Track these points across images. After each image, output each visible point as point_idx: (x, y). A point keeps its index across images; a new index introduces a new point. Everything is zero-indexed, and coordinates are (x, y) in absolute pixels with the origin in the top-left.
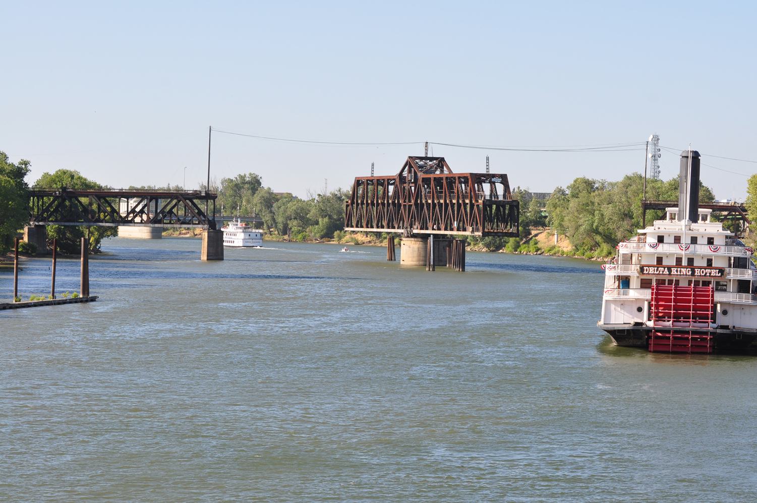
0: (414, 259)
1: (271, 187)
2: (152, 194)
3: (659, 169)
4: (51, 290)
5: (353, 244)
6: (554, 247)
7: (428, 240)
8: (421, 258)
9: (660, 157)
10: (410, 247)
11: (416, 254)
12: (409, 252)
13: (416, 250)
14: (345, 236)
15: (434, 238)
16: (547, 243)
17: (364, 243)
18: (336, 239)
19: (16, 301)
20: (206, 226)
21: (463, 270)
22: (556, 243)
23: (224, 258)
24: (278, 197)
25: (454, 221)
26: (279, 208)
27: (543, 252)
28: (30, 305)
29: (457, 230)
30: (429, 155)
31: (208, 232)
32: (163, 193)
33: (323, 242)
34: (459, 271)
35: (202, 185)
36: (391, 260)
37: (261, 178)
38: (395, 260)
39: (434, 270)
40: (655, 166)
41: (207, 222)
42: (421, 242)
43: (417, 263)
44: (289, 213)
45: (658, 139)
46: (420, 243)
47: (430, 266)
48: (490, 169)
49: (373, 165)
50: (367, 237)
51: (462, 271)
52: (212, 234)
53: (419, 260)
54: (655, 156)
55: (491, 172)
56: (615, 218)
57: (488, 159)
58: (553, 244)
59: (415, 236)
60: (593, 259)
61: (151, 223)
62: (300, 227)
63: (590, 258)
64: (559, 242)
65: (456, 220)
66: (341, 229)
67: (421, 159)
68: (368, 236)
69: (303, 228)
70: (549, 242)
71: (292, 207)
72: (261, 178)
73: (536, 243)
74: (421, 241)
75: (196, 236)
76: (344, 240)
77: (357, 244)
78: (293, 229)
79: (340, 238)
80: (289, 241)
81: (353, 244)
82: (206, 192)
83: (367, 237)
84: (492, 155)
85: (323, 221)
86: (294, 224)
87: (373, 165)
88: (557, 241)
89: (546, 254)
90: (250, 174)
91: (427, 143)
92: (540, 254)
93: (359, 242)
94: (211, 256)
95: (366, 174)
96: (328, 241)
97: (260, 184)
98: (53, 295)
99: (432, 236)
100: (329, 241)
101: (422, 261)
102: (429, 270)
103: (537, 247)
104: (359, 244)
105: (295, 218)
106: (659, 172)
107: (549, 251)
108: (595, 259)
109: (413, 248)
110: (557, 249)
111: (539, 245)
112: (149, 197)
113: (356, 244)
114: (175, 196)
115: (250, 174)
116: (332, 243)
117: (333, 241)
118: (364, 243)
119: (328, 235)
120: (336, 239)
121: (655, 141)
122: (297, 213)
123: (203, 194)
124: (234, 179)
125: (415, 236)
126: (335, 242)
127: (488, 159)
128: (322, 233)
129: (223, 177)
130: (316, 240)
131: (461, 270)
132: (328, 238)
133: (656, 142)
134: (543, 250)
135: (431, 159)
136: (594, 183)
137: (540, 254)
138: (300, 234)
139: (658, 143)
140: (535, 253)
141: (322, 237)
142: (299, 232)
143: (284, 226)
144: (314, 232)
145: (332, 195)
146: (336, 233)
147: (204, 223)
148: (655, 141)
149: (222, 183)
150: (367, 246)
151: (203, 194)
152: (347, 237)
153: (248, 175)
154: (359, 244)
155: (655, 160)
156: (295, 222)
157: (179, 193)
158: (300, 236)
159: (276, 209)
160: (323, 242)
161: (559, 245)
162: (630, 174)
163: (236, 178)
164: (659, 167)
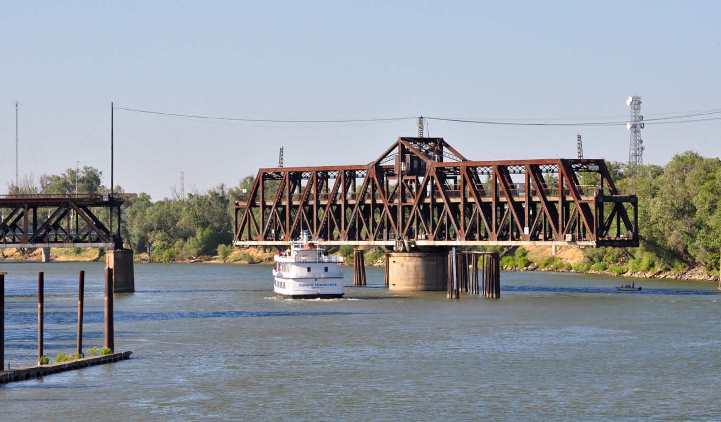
0: (410, 283)
1: (121, 186)
2: (32, 202)
3: (643, 145)
4: (38, 344)
5: (246, 262)
6: (552, 260)
7: (449, 256)
8: (420, 281)
9: (643, 128)
10: (402, 265)
11: (412, 275)
12: (402, 272)
13: (412, 269)
14: (232, 252)
15: (457, 251)
16: (540, 254)
17: (261, 261)
18: (220, 255)
19: (42, 363)
20: (111, 244)
21: (498, 296)
22: (554, 253)
23: (136, 289)
24: (130, 199)
25: (523, 226)
26: (134, 214)
27: (537, 267)
28: (64, 367)
29: (531, 240)
30: (425, 136)
31: (115, 253)
32: (44, 199)
33: (201, 261)
34: (492, 297)
35: (12, 185)
36: (361, 284)
37: (101, 173)
38: (365, 284)
39: (458, 297)
40: (635, 140)
41: (112, 239)
42: (418, 258)
43: (414, 288)
44: (150, 221)
45: (640, 103)
46: (417, 261)
47: (452, 290)
48: (284, 152)
49: (282, 150)
50: (265, 252)
51: (496, 297)
52: (120, 255)
53: (416, 284)
54: (635, 127)
55: (586, 157)
56: (668, 216)
57: (579, 137)
58: (549, 255)
59: (416, 249)
60: (625, 275)
61: (31, 243)
62: (165, 240)
63: (620, 274)
64: (559, 252)
65: (526, 224)
66: (228, 241)
67: (415, 140)
68: (267, 251)
69: (169, 242)
70: (544, 252)
71: (150, 217)
72: (101, 173)
73: (524, 255)
74: (420, 257)
75: (7, 259)
76: (231, 258)
77: (252, 262)
78: (154, 245)
79: (226, 254)
80: (150, 261)
81: (246, 262)
82: (109, 195)
83: (265, 252)
84: (584, 132)
85: (200, 234)
86: (156, 240)
87: (282, 150)
88: (556, 251)
89: (543, 269)
90: (86, 168)
91: (422, 118)
92: (533, 270)
93: (255, 260)
94: (119, 287)
95: (271, 163)
96: (207, 260)
97: (98, 181)
98: (80, 352)
99: (454, 249)
100: (209, 260)
101: (421, 284)
102: (451, 298)
103: (527, 260)
104: (254, 263)
105: (159, 229)
106: (643, 149)
107: (546, 265)
108: (628, 274)
109: (408, 266)
110: (558, 262)
111: (529, 257)
112: (26, 206)
113: (251, 263)
114: (64, 203)
115: (86, 168)
116: (213, 262)
117: (215, 259)
118: (261, 261)
119: (208, 250)
120: (220, 255)
121: (635, 105)
122: (160, 221)
123: (106, 199)
124: (61, 176)
125: (416, 249)
126: (218, 260)
127: (579, 137)
128: (200, 249)
129: (42, 174)
130: (190, 258)
131: (495, 295)
132: (208, 255)
133: (636, 107)
134: (536, 264)
135: (427, 141)
136: (618, 167)
137: (533, 270)
138: (165, 250)
139: (639, 108)
140: (525, 268)
141: (199, 254)
142: (163, 248)
143: (140, 241)
144: (191, 246)
145: (212, 194)
146: (221, 248)
147: (107, 240)
148: (635, 105)
149: (42, 181)
150: (266, 265)
151: (106, 199)
152: (236, 253)
153: (82, 169)
154: (254, 263)
155: (636, 132)
156: (159, 235)
157: (71, 199)
158: (165, 254)
159: (129, 216)
160: (201, 261)
161: (560, 256)
162: (681, 153)
163: (64, 175)
164: (641, 142)
